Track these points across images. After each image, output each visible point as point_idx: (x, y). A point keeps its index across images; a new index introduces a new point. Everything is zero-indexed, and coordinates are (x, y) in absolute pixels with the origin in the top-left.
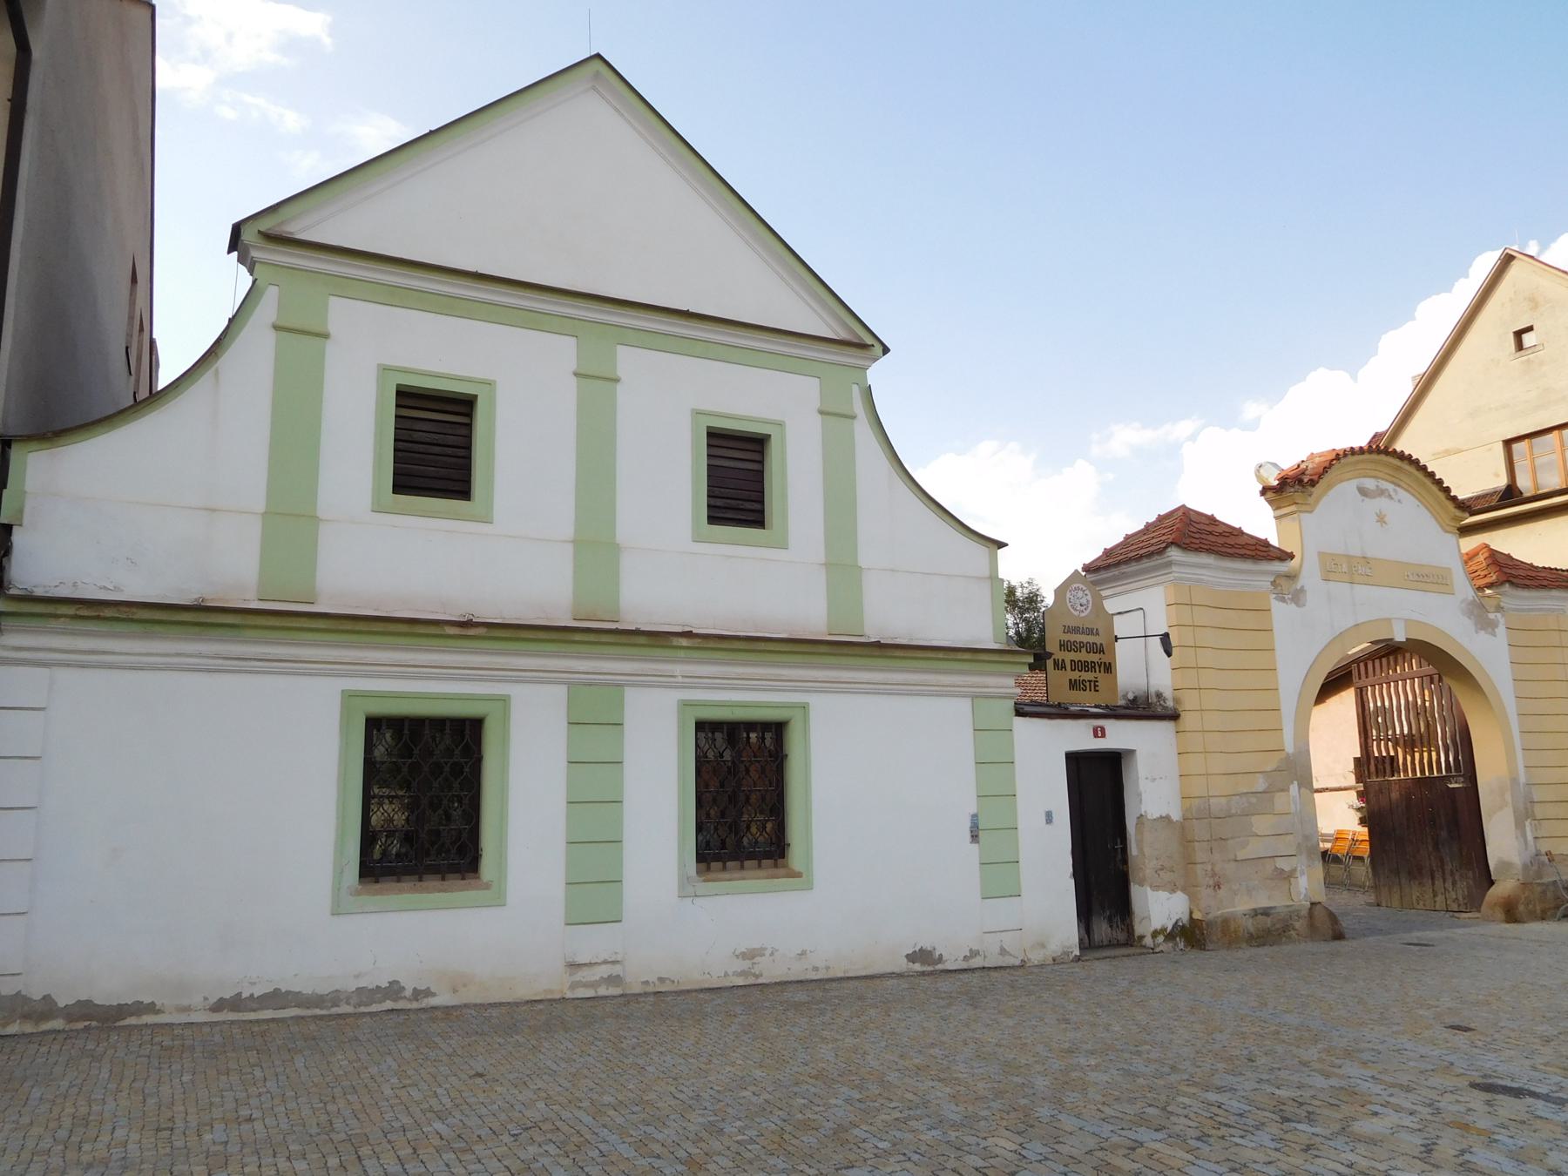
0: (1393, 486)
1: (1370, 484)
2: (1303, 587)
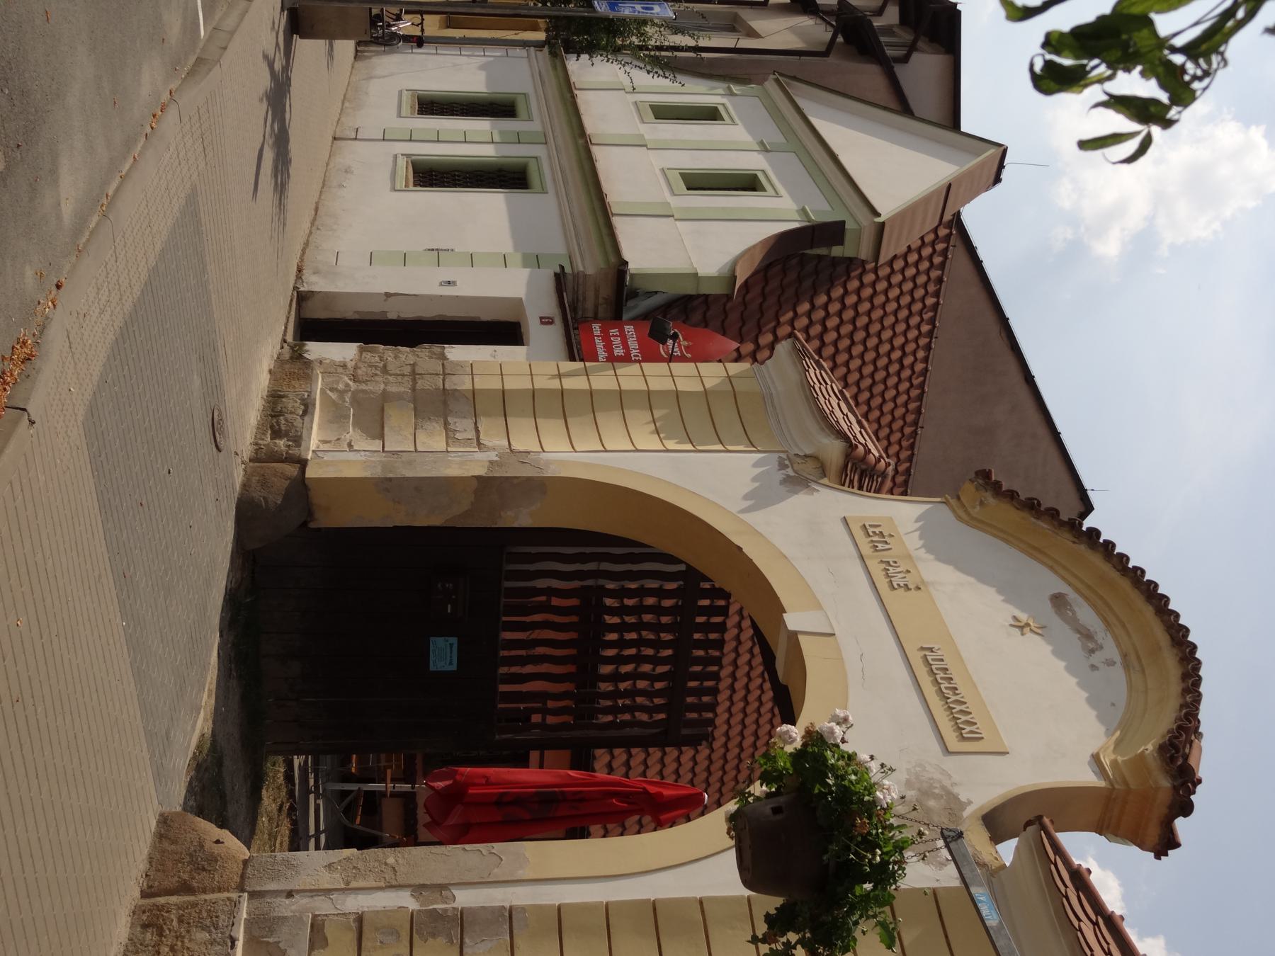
1: (1086, 615)
2: (818, 491)
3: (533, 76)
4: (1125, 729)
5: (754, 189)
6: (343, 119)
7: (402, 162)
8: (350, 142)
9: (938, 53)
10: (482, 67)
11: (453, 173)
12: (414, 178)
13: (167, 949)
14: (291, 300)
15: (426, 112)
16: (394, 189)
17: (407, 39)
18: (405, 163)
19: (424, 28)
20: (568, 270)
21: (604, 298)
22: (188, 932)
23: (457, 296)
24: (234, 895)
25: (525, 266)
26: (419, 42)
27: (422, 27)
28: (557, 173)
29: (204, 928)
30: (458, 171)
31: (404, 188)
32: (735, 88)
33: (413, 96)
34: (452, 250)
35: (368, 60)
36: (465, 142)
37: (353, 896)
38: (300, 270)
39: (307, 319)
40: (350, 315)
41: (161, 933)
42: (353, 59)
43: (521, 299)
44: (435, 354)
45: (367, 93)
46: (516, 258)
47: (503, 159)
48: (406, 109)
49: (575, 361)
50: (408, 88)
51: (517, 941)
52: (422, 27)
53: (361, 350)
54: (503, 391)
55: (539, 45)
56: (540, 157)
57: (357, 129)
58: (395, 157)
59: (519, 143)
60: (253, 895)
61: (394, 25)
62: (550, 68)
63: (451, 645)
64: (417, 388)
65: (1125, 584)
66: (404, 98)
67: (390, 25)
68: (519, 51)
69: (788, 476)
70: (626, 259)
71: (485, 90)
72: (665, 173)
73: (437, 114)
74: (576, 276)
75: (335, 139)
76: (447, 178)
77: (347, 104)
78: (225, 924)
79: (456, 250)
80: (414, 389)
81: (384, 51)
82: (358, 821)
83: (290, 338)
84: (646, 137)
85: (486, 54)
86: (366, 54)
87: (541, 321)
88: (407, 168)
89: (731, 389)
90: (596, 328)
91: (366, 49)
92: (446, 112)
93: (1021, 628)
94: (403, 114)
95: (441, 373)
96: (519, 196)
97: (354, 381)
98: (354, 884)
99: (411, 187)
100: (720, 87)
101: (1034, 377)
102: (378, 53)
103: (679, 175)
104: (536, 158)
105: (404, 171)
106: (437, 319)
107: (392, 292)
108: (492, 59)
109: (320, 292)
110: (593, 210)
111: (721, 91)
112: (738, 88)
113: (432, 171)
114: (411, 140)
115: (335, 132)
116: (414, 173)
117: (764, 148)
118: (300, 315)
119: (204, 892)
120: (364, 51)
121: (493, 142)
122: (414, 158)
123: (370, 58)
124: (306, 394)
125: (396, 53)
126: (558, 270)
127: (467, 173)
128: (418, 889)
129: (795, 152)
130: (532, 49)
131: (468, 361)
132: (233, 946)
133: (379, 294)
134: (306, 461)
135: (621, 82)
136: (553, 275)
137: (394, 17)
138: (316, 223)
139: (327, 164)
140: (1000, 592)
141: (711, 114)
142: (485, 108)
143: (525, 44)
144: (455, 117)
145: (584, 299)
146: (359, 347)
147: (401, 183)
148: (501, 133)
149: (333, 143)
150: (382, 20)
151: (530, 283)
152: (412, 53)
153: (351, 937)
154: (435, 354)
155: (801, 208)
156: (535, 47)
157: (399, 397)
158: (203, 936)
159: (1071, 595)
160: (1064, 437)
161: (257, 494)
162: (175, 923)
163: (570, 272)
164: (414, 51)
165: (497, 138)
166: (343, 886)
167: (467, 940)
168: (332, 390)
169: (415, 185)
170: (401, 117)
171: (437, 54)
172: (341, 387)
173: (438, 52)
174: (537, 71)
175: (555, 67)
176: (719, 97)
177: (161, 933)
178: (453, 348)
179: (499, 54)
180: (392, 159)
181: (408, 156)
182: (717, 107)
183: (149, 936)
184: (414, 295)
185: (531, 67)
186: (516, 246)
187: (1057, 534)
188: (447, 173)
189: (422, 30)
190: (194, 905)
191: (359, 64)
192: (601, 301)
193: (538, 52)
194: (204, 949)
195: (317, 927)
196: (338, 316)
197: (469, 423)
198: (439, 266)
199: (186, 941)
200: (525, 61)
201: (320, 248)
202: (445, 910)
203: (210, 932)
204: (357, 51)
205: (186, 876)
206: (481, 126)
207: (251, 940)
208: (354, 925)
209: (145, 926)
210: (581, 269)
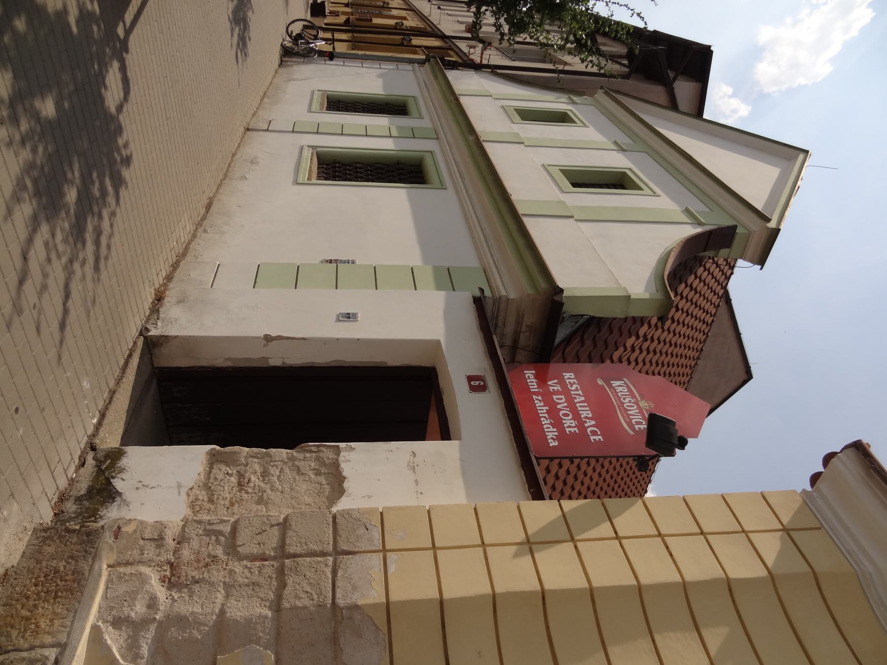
3: (418, 83)
5: (623, 187)
6: (260, 112)
7: (307, 153)
8: (261, 133)
9: (692, 82)
10: (379, 76)
11: (355, 165)
12: (318, 170)
14: (130, 356)
15: (333, 108)
16: (296, 183)
17: (321, 54)
18: (310, 154)
19: (335, 47)
20: (488, 293)
21: (527, 326)
23: (358, 340)
25: (439, 287)
26: (331, 56)
27: (334, 46)
28: (452, 167)
30: (359, 163)
31: (306, 181)
32: (575, 98)
33: (323, 95)
34: (353, 262)
35: (290, 68)
36: (367, 135)
38: (159, 298)
39: (164, 368)
40: (220, 363)
42: (277, 66)
43: (436, 345)
44: (325, 465)
45: (285, 92)
46: (426, 276)
47: (403, 152)
48: (316, 106)
49: (544, 499)
50: (318, 89)
52: (334, 46)
53: (213, 460)
54: (441, 602)
55: (421, 63)
56: (434, 151)
57: (270, 121)
58: (302, 148)
59: (414, 137)
61: (312, 43)
62: (432, 78)
64: (286, 605)
66: (315, 97)
67: (309, 43)
68: (409, 67)
70: (561, 285)
71: (382, 93)
72: (547, 169)
73: (342, 111)
74: (497, 301)
75: (248, 130)
76: (349, 170)
77: (266, 100)
79: (358, 262)
80: (277, 607)
81: (303, 62)
84: (522, 135)
85: (381, 67)
86: (289, 63)
87: (470, 386)
88: (311, 159)
89: (809, 570)
91: (290, 59)
92: (350, 110)
94: (313, 109)
95: (330, 548)
96: (419, 191)
99: (314, 181)
100: (564, 98)
101: (731, 300)
102: (298, 63)
103: (559, 171)
104: (431, 152)
105: (309, 163)
106: (333, 364)
107: (273, 335)
108: (386, 71)
109: (176, 337)
110: (499, 211)
111: (564, 100)
112: (576, 98)
113: (335, 163)
114: (317, 133)
115: (249, 124)
116: (319, 164)
117: (621, 149)
118: (152, 364)
120: (287, 61)
121: (391, 136)
122: (319, 149)
123: (292, 66)
125: (313, 63)
127: (368, 165)
129: (646, 152)
130: (416, 64)
131: (378, 509)
133: (259, 338)
135: (488, 91)
136: (472, 299)
137: (313, 38)
138: (205, 223)
139: (233, 155)
141: (562, 118)
142: (382, 107)
143: (410, 61)
144: (357, 113)
145: (504, 324)
146: (212, 455)
147: (303, 176)
148: (399, 128)
149: (245, 133)
150: (302, 38)
151: (448, 313)
152: (325, 64)
154: (325, 465)
155: (684, 208)
156: (418, 63)
160: (743, 337)
163: (490, 295)
164: (327, 62)
165: (394, 133)
168: (117, 623)
169: (319, 178)
170: (311, 112)
171: (344, 65)
172: (139, 609)
173: (345, 64)
174: (423, 80)
175: (436, 78)
176: (565, 105)
178: (352, 449)
179: (391, 67)
180: (298, 150)
181: (314, 147)
182: (566, 112)
184: (303, 339)
185: (416, 76)
186: (426, 256)
188: (350, 165)
189: (334, 48)
191: (283, 70)
192: (524, 328)
193: (421, 68)
196: (204, 363)
198: (336, 288)
200: (411, 73)
201: (199, 260)
204: (282, 61)
206: (381, 121)
210: (504, 293)
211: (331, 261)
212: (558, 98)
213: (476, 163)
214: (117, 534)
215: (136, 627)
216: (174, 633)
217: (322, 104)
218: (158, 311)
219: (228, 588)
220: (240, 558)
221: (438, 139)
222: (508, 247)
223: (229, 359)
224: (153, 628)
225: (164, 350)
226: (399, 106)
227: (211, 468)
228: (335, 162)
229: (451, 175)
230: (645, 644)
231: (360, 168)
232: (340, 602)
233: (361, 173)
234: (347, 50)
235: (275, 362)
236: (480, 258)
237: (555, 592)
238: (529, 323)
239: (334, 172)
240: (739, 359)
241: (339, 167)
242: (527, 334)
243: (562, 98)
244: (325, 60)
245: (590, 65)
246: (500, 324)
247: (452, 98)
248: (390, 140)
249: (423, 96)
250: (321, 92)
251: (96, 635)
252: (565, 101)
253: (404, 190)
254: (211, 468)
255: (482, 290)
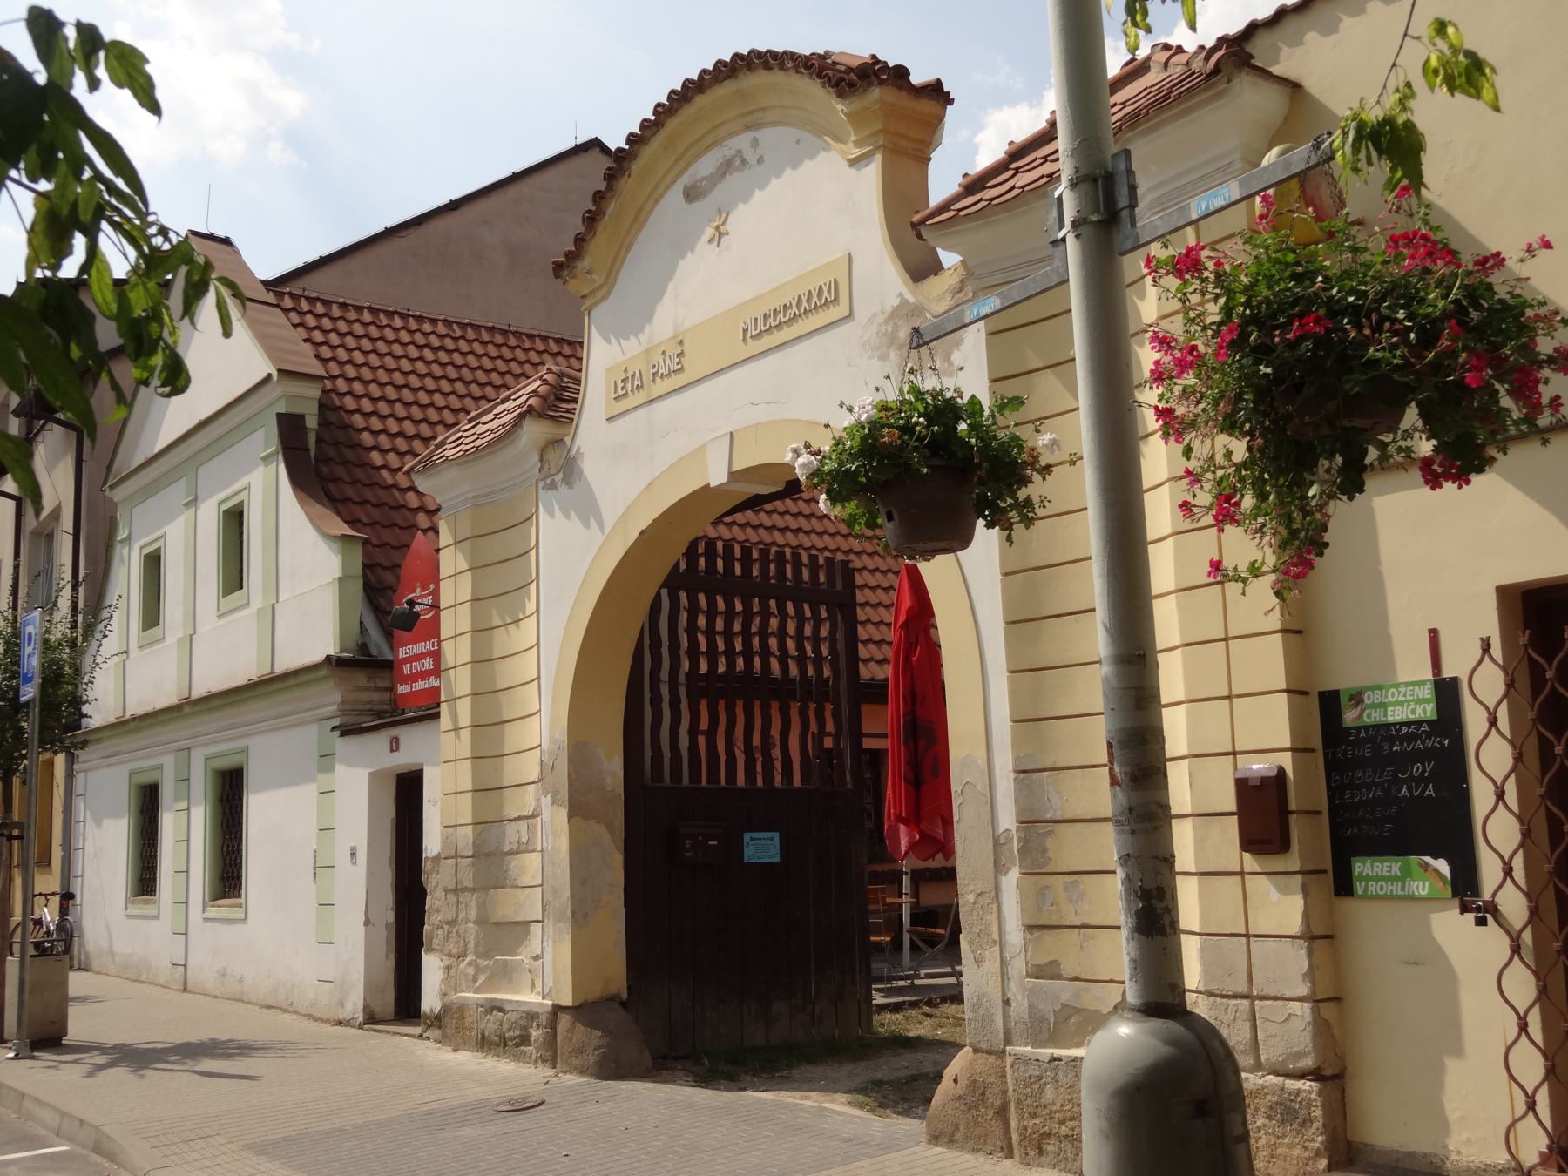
0: (750, 135)
1: (706, 165)
2: (579, 448)
4: (823, 131)
5: (241, 514)
6: (162, 981)
7: (212, 912)
8: (189, 973)
10: (99, 823)
13: (1063, 1128)
16: (244, 920)
17: (64, 911)
20: (336, 722)
22: (1045, 1107)
24: (1009, 1061)
25: (331, 769)
26: (67, 897)
29: (1042, 1090)
34: (315, 852)
36: (188, 841)
37: (1007, 937)
38: (340, 1023)
40: (391, 964)
41: (1048, 1135)
42: (89, 973)
43: (371, 774)
46: (324, 780)
48: (150, 910)
51: (1048, 764)
53: (431, 950)
58: (206, 920)
60: (1008, 1041)
61: (48, 927)
63: (752, 839)
64: (472, 886)
65: (672, 124)
67: (48, 933)
68: (80, 779)
69: (563, 480)
73: (155, 874)
77: (144, 978)
78: (1037, 1068)
80: (474, 890)
82: (941, 931)
83: (417, 1030)
86: (83, 958)
90: (403, 689)
93: (721, 235)
94: (155, 912)
96: (251, 778)
97: (465, 956)
98: (996, 936)
99: (242, 900)
100: (120, 552)
105: (224, 909)
106: (394, 866)
107: (363, 918)
108: (88, 813)
113: (223, 878)
115: (178, 990)
116: (225, 898)
117: (193, 502)
119: (1006, 1092)
121: (188, 809)
122: (207, 899)
123: (87, 954)
124: (480, 1009)
125: (81, 922)
126: (337, 733)
128: (999, 868)
130: (75, 767)
132: (1059, 1059)
134: (554, 1006)
137: (38, 927)
140: (683, 256)
141: (153, 562)
143: (70, 775)
145: (369, 703)
147: (237, 913)
148: (177, 799)
149: (190, 992)
151: (352, 763)
153: (1047, 936)
156: (73, 764)
157: (482, 907)
158: (1049, 1092)
159: (685, 180)
161: (591, 1058)
162: (1037, 1121)
164: (78, 903)
165: (184, 805)
166: (998, 947)
167: (1048, 816)
168: (475, 981)
172: (471, 971)
177: (1048, 1135)
179: (82, 805)
183: (1050, 1148)
187: (621, 193)
188: (225, 860)
189: (53, 894)
190: (1019, 1102)
191: (95, 965)
192: (371, 684)
193: (80, 760)
194: (1062, 1089)
195: (1038, 972)
196: (391, 977)
197: (510, 828)
199: (1054, 1108)
202: (1019, 840)
203: (1045, 1084)
204: (79, 969)
205: (991, 1113)
206: (168, 823)
207: (1053, 1041)
208: (1036, 934)
209: (1041, 1152)
211: (315, 874)
212: (122, 561)
213: (217, 708)
214: (444, 994)
215: (478, 970)
216: (480, 949)
217: (147, 903)
218: (348, 1021)
219: (468, 921)
220: (458, 917)
221: (189, 749)
222: (623, 248)
223: (387, 957)
224: (479, 961)
225: (377, 1010)
226: (145, 796)
227: (434, 950)
228: (222, 878)
229: (232, 739)
230: (497, 664)
231: (228, 847)
232: (470, 854)
233: (233, 847)
234: (50, 873)
235: (391, 917)
236: (311, 722)
237: (472, 721)
238: (365, 680)
239: (233, 879)
240: (561, 168)
241: (228, 873)
242: (377, 680)
243: (122, 556)
244: (73, 905)
245: (109, 627)
246: (368, 707)
247: (132, 724)
248: (193, 811)
249: (128, 761)
250: (129, 905)
251: (477, 991)
252: (125, 551)
253: (250, 797)
254: (434, 950)
255: (334, 728)
